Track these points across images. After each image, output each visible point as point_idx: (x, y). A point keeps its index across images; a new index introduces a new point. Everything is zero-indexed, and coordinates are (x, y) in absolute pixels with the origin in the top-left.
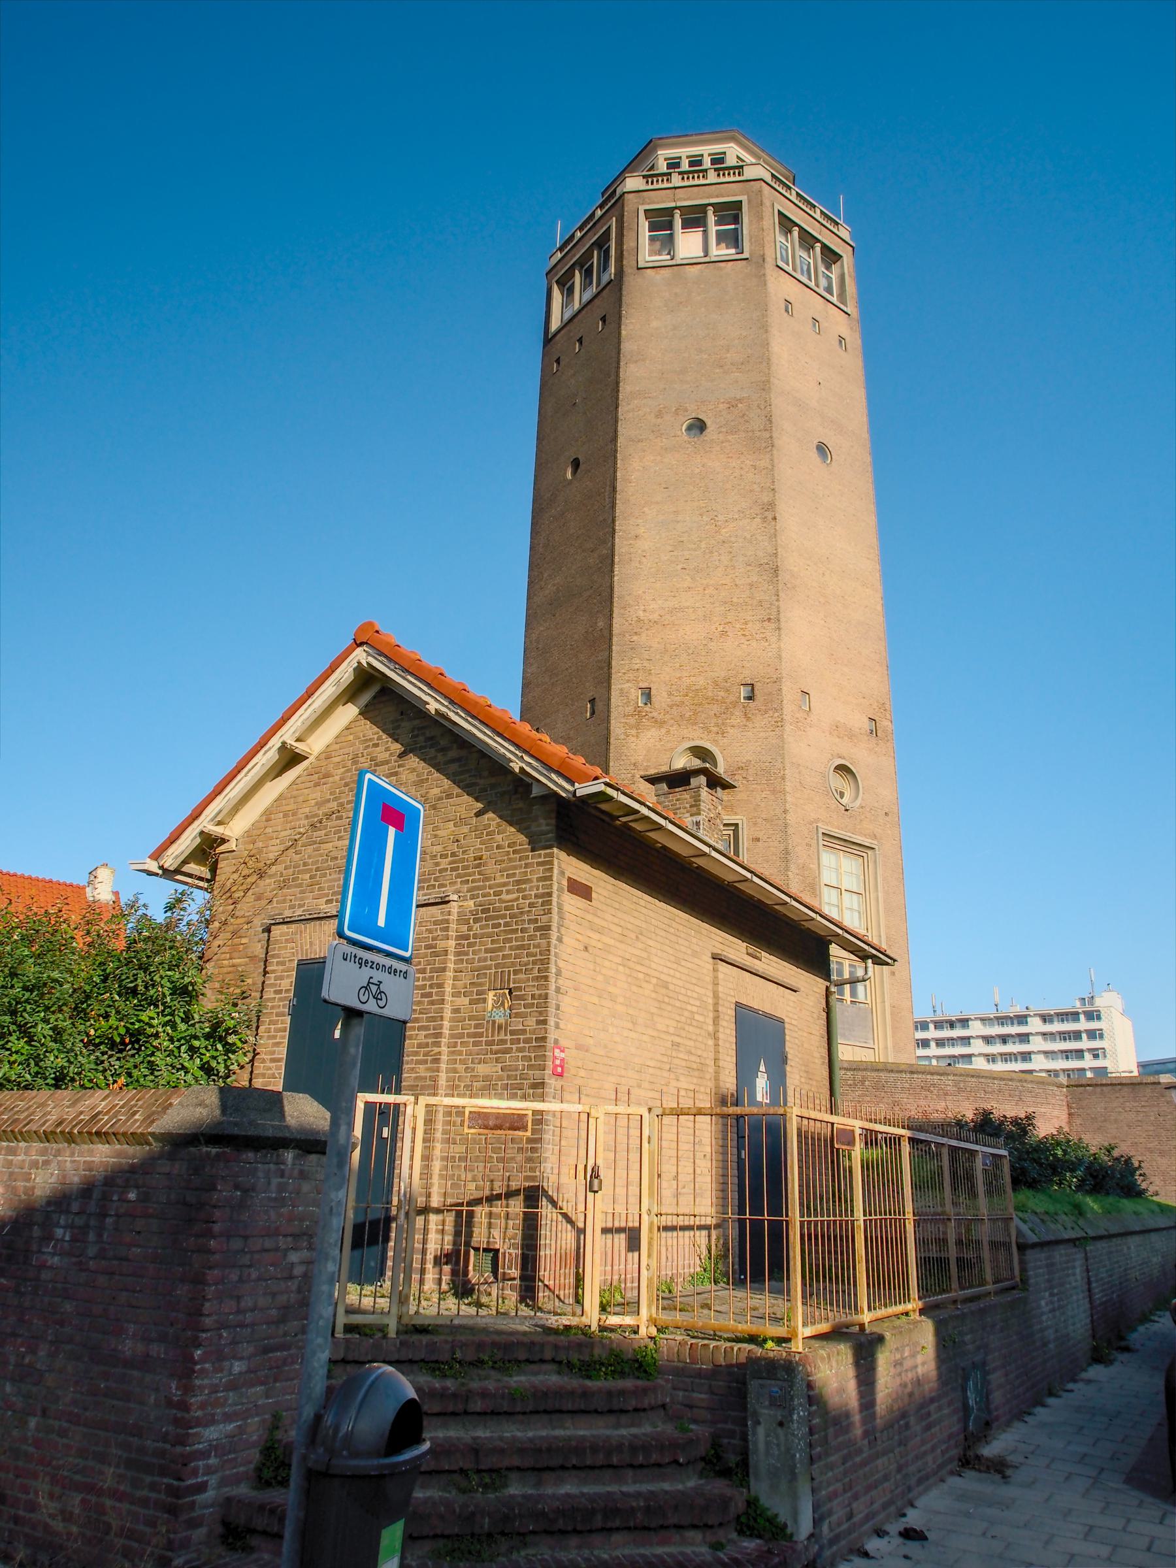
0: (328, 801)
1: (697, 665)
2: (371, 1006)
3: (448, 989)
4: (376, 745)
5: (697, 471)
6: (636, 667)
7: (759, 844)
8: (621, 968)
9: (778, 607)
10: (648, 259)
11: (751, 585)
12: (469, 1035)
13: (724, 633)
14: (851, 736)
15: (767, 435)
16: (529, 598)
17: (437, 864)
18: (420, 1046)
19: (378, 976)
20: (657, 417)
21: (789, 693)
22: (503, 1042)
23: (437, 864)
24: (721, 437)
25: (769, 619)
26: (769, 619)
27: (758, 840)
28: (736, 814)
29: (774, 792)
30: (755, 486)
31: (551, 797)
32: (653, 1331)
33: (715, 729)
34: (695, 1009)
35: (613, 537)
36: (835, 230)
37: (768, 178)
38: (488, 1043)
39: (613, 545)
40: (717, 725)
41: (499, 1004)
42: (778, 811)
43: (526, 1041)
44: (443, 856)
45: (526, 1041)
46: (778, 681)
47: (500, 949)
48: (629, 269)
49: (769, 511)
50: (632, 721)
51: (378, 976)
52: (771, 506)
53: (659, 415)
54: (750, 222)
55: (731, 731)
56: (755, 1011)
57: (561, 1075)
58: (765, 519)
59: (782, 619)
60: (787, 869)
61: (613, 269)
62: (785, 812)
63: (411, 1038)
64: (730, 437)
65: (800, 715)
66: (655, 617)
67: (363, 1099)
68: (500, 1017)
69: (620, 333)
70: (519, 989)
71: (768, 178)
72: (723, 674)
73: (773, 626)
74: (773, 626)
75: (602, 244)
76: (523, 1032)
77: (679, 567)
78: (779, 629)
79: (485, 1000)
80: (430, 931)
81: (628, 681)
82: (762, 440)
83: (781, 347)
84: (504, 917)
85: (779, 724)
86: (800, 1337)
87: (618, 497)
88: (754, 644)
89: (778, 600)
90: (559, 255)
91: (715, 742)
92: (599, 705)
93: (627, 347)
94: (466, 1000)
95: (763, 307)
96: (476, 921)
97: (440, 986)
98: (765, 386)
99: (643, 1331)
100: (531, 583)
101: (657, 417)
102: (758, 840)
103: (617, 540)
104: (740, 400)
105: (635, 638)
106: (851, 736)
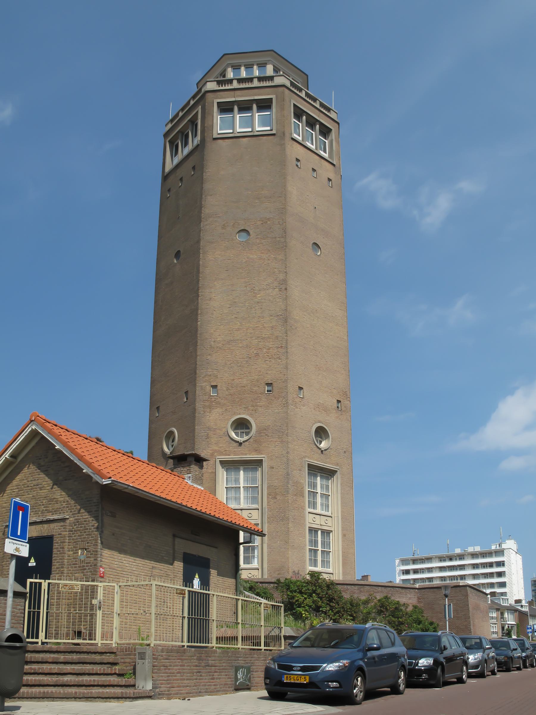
0: (24, 480)
1: (242, 373)
2: (17, 554)
3: (66, 549)
4: (40, 459)
5: (244, 261)
6: (210, 373)
7: (274, 470)
8: (129, 541)
9: (287, 340)
10: (219, 132)
11: (272, 327)
12: (73, 564)
13: (257, 355)
14: (326, 410)
15: (282, 240)
16: (154, 332)
17: (62, 505)
18: (57, 568)
19: (18, 546)
20: (223, 228)
21: (292, 388)
22: (84, 566)
23: (62, 505)
24: (258, 241)
25: (282, 347)
26: (282, 347)
27: (273, 468)
28: (262, 454)
29: (282, 442)
30: (276, 270)
31: (97, 483)
32: (116, 645)
33: (251, 408)
34: (164, 555)
35: (198, 299)
36: (328, 114)
37: (288, 84)
38: (80, 567)
39: (198, 303)
40: (253, 406)
41: (82, 554)
42: (284, 452)
43: (91, 566)
44: (64, 502)
45: (91, 566)
46: (286, 381)
47: (83, 535)
48: (208, 139)
49: (283, 286)
50: (207, 404)
51: (18, 546)
52: (284, 282)
53: (224, 227)
54: (277, 111)
55: (260, 409)
56: (195, 556)
57: (102, 577)
58: (280, 290)
59: (289, 347)
60: (288, 483)
61: (199, 138)
62: (288, 453)
63: (54, 565)
64: (263, 241)
65: (298, 400)
66: (220, 345)
67: (29, 581)
68: (82, 558)
69: (203, 178)
70: (88, 549)
71: (288, 84)
72: (256, 377)
73: (284, 351)
74: (284, 351)
75: (193, 122)
76: (89, 563)
77: (233, 317)
78: (287, 352)
79: (78, 553)
80: (59, 529)
81: (205, 381)
82: (281, 244)
83: (293, 189)
84: (84, 524)
85: (286, 405)
86: (42, 581)
87: (201, 275)
88: (273, 361)
89: (286, 336)
90: (170, 126)
91: (251, 415)
92: (190, 395)
93: (207, 186)
94: (72, 553)
95: (283, 163)
96: (75, 525)
97: (63, 548)
98: (283, 211)
99: (114, 646)
100: (155, 323)
101: (223, 228)
102: (273, 468)
103: (200, 301)
104: (269, 219)
105: (209, 357)
106: (326, 410)
